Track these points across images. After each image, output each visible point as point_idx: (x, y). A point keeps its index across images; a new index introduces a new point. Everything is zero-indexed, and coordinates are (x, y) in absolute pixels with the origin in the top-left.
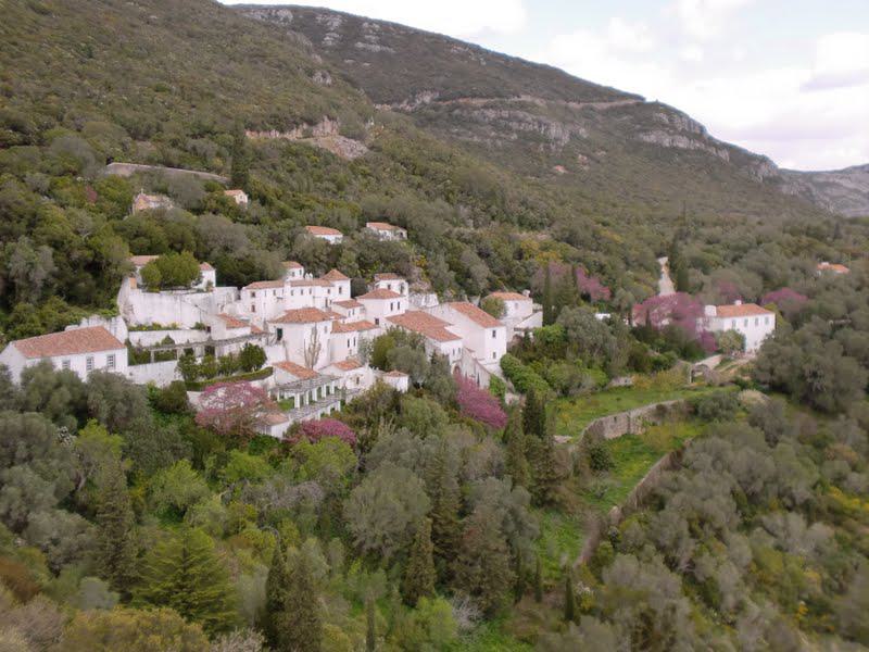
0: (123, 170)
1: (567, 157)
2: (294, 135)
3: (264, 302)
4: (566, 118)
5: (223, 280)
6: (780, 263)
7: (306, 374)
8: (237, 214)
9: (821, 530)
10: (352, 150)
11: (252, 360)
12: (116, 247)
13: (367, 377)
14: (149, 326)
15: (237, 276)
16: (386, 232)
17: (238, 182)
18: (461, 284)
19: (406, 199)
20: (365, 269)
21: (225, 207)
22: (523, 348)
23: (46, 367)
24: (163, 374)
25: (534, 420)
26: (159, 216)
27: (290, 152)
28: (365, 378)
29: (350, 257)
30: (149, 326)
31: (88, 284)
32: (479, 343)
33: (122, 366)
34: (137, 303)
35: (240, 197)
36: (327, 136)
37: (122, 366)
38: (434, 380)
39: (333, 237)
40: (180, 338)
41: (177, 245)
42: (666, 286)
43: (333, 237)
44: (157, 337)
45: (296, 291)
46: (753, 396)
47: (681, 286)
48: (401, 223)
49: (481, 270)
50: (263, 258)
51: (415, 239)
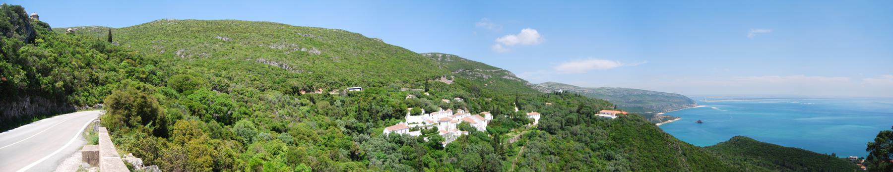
0: (403, 90)
1: (487, 82)
2: (437, 80)
3: (435, 117)
4: (487, 73)
5: (426, 112)
6: (539, 104)
7: (447, 134)
8: (428, 98)
9: (557, 157)
10: (449, 82)
11: (435, 130)
12: (404, 106)
13: (459, 133)
14: (411, 125)
15: (429, 112)
16: (458, 99)
17: (427, 91)
18: (475, 111)
19: (462, 92)
20: (456, 108)
21: (425, 96)
22: (490, 123)
23: (393, 132)
24: (418, 134)
25: (497, 140)
26: (412, 99)
27: (436, 84)
28: (459, 133)
29: (452, 105)
30: (411, 125)
31: (400, 114)
32: (481, 123)
33: (408, 132)
34: (409, 118)
35: (427, 94)
36: (443, 80)
37: (408, 132)
38: (473, 130)
39: (447, 101)
40: (420, 125)
41: (417, 105)
42: (517, 109)
43: (447, 101)
44: (414, 126)
45: (440, 115)
46: (538, 131)
47: (520, 109)
48: (461, 97)
49: (479, 107)
50: (434, 107)
51: (465, 101)
